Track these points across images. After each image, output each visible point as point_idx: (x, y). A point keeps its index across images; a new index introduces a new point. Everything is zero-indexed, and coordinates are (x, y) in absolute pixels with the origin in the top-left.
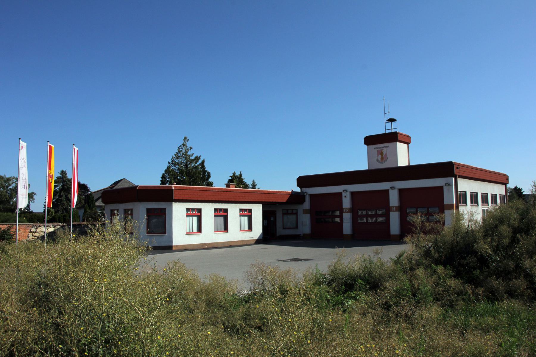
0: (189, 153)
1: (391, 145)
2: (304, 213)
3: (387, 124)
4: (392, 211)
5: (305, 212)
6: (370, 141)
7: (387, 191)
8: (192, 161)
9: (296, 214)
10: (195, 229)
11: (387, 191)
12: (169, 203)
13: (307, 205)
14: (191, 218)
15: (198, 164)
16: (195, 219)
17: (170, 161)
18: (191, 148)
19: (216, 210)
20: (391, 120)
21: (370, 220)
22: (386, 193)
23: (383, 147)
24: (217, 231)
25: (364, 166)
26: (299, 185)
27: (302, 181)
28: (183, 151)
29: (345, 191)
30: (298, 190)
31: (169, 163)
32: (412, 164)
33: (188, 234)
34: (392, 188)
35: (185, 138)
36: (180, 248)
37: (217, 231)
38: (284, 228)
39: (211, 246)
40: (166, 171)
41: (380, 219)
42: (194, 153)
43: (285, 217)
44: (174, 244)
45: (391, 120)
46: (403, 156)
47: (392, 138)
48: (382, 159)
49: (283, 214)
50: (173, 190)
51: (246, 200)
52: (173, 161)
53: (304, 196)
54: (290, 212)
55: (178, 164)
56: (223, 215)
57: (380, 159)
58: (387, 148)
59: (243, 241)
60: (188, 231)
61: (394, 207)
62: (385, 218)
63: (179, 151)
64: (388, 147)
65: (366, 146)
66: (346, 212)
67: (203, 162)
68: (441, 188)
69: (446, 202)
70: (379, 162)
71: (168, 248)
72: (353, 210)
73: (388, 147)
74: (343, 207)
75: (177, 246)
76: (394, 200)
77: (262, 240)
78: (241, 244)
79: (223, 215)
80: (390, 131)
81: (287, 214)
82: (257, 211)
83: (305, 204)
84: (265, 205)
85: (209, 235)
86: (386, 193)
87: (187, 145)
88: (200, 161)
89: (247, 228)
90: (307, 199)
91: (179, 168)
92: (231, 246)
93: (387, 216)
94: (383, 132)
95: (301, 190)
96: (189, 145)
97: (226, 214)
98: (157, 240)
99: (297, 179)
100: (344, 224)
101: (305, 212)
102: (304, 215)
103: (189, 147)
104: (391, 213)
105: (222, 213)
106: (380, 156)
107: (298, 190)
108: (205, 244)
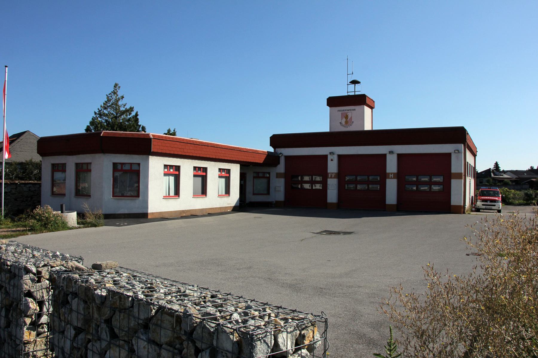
0: (120, 103)
1: (357, 108)
2: (277, 177)
3: (349, 86)
4: (389, 178)
5: (278, 175)
6: (333, 102)
7: (384, 156)
8: (123, 113)
9: (269, 178)
10: (172, 193)
11: (384, 156)
12: (145, 156)
13: (281, 168)
14: (167, 177)
15: (131, 116)
16: (172, 179)
17: (97, 111)
18: (123, 97)
19: (195, 168)
20: (355, 82)
21: (359, 187)
22: (383, 157)
23: (348, 110)
24: (195, 195)
25: (326, 129)
26: (272, 145)
27: (277, 141)
28: (112, 101)
29: (332, 153)
30: (272, 150)
31: (95, 113)
32: (374, 129)
33: (165, 197)
34: (391, 152)
35: (116, 85)
36: (157, 216)
37: (195, 195)
38: (254, 194)
39: (189, 214)
40: (91, 123)
41: (435, 188)
42: (126, 103)
43: (255, 180)
44: (150, 211)
45: (355, 82)
46: (370, 121)
47: (361, 100)
48: (346, 122)
49: (254, 177)
50: (151, 139)
51: (226, 158)
52: (100, 111)
53: (279, 158)
54: (261, 175)
55: (106, 115)
56: (201, 175)
57: (344, 123)
58: (353, 111)
59: (221, 208)
60: (220, 194)
61: (391, 173)
62: (442, 186)
63: (109, 100)
64: (355, 110)
65: (328, 108)
66: (331, 177)
67: (137, 115)
68: (449, 155)
69: (453, 170)
70: (343, 126)
71: (142, 217)
72: (400, 176)
73: (355, 110)
74: (329, 171)
75: (153, 213)
76: (392, 166)
77: (237, 209)
78: (219, 211)
79: (201, 175)
80: (353, 94)
81: (258, 177)
82: (235, 170)
83: (279, 166)
84: (245, 166)
85: (188, 201)
86: (324, 158)
87: (118, 93)
88: (133, 114)
89: (224, 193)
90: (282, 161)
91: (106, 121)
92: (210, 215)
93: (324, 183)
94: (346, 94)
95: (275, 150)
96: (120, 94)
97: (177, 173)
98: (126, 206)
99: (271, 138)
100: (328, 191)
101: (278, 175)
102: (277, 179)
103: (120, 95)
104: (388, 181)
105: (200, 173)
106: (344, 120)
107: (272, 150)
108: (183, 211)
